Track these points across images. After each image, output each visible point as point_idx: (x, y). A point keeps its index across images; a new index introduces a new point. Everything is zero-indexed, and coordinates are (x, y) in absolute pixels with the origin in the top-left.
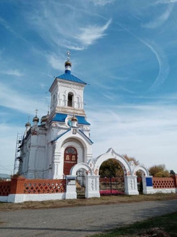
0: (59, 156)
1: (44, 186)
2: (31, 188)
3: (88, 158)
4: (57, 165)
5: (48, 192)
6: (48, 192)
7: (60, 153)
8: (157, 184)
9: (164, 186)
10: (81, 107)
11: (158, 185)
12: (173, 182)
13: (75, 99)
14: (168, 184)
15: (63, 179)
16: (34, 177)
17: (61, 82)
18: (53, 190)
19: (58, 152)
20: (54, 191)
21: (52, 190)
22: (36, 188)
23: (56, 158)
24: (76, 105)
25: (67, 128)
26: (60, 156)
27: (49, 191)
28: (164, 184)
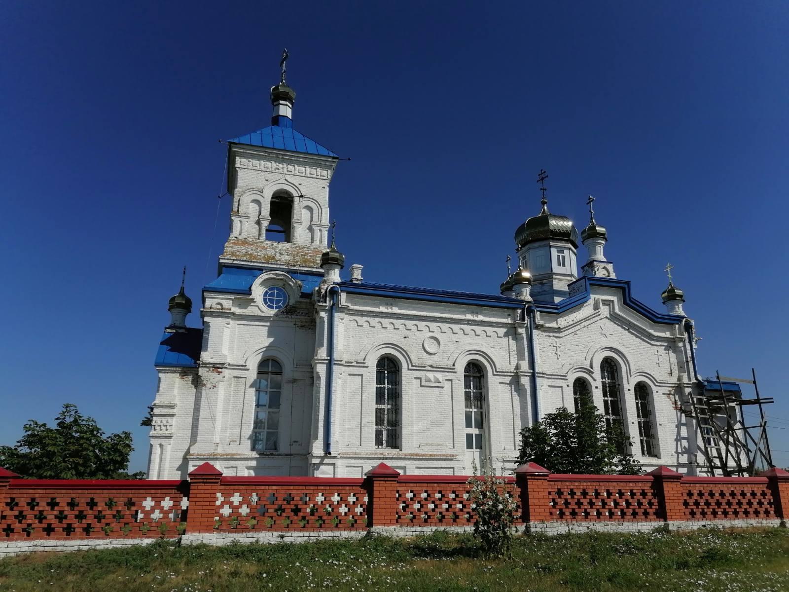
0: (169, 419)
1: (289, 503)
2: (292, 510)
3: (686, 389)
4: (161, 445)
5: (321, 526)
6: (321, 526)
7: (172, 407)
8: (713, 502)
9: (730, 511)
10: (321, 242)
11: (724, 506)
12: (764, 494)
13: (300, 215)
14: (755, 502)
15: (727, 467)
16: (324, 472)
17: (242, 155)
18: (426, 513)
19: (166, 402)
20: (429, 517)
21: (467, 516)
22: (25, 517)
23: (159, 422)
24: (300, 234)
25: (260, 314)
26: (173, 415)
27: (324, 521)
28: (740, 504)
